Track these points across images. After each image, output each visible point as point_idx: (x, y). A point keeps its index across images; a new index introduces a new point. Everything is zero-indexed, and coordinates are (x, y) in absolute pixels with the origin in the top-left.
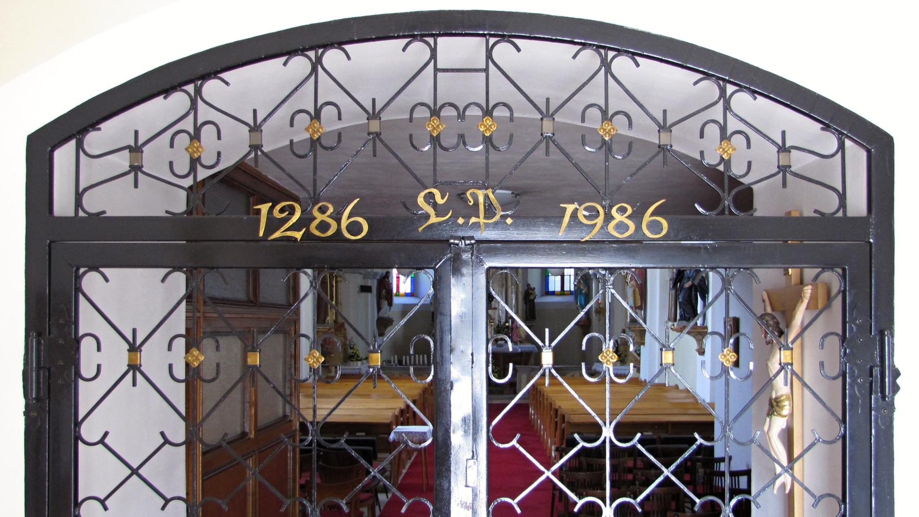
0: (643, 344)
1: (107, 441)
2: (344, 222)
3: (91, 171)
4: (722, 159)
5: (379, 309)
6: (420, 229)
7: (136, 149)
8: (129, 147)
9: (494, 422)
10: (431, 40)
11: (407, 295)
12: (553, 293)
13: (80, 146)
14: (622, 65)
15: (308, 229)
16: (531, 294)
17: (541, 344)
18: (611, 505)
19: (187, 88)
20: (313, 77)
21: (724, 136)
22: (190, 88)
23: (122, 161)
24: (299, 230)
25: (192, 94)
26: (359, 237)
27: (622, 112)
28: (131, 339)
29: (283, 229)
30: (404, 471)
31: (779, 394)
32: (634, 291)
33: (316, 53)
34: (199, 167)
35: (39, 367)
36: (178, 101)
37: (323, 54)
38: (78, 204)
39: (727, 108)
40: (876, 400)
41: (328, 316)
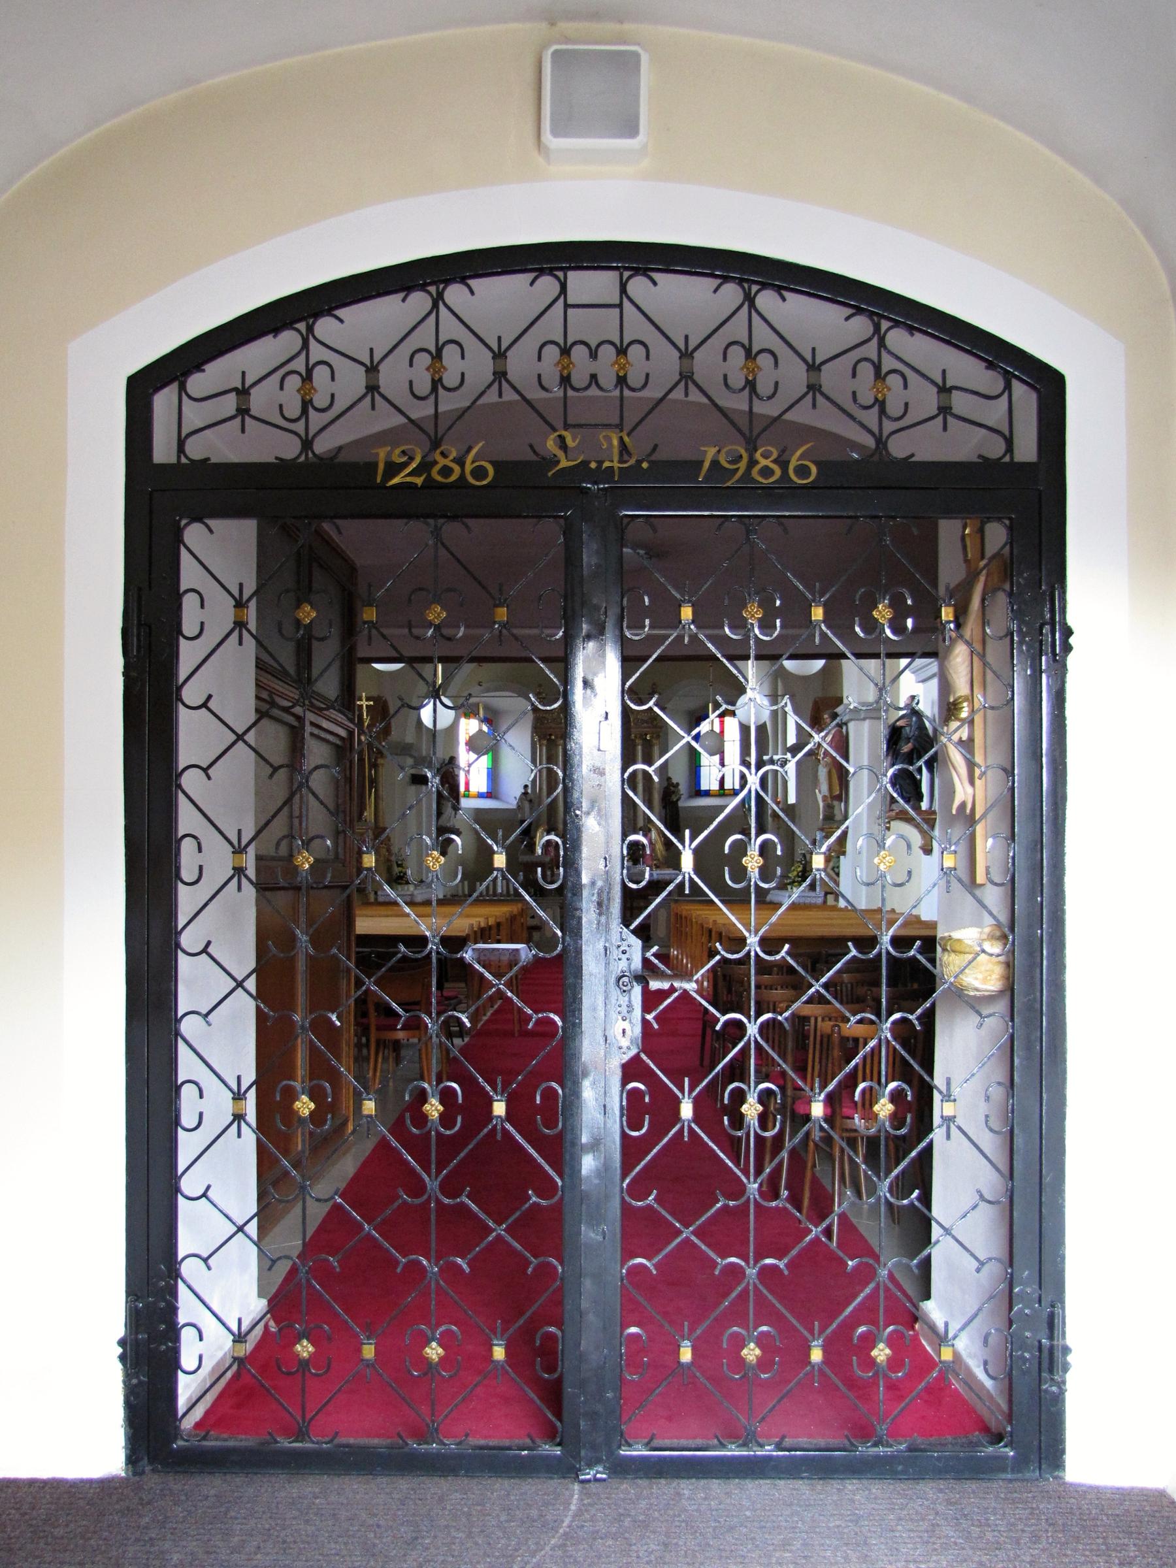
0: (844, 853)
1: (210, 705)
2: (469, 467)
3: (194, 415)
4: (876, 400)
5: (439, 814)
6: (550, 474)
7: (243, 392)
8: (235, 389)
9: (628, 684)
10: (560, 274)
11: (480, 795)
12: (707, 793)
13: (182, 388)
14: (766, 300)
15: (429, 475)
16: (674, 792)
17: (693, 1125)
18: (756, 774)
19: (298, 326)
20: (434, 315)
21: (879, 375)
22: (302, 326)
23: (229, 404)
24: (420, 476)
25: (304, 332)
26: (485, 482)
27: (987, 1126)
28: (237, 595)
29: (402, 474)
30: (485, 1018)
31: (958, 694)
32: (830, 773)
33: (438, 288)
34: (311, 410)
35: (139, 625)
36: (288, 341)
37: (444, 289)
38: (181, 449)
39: (882, 344)
40: (1047, 661)
41: (365, 809)
